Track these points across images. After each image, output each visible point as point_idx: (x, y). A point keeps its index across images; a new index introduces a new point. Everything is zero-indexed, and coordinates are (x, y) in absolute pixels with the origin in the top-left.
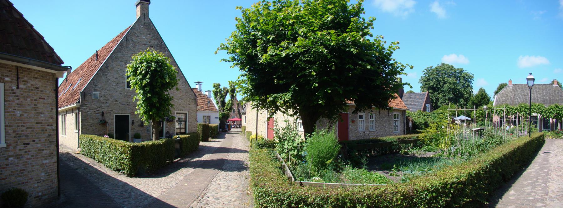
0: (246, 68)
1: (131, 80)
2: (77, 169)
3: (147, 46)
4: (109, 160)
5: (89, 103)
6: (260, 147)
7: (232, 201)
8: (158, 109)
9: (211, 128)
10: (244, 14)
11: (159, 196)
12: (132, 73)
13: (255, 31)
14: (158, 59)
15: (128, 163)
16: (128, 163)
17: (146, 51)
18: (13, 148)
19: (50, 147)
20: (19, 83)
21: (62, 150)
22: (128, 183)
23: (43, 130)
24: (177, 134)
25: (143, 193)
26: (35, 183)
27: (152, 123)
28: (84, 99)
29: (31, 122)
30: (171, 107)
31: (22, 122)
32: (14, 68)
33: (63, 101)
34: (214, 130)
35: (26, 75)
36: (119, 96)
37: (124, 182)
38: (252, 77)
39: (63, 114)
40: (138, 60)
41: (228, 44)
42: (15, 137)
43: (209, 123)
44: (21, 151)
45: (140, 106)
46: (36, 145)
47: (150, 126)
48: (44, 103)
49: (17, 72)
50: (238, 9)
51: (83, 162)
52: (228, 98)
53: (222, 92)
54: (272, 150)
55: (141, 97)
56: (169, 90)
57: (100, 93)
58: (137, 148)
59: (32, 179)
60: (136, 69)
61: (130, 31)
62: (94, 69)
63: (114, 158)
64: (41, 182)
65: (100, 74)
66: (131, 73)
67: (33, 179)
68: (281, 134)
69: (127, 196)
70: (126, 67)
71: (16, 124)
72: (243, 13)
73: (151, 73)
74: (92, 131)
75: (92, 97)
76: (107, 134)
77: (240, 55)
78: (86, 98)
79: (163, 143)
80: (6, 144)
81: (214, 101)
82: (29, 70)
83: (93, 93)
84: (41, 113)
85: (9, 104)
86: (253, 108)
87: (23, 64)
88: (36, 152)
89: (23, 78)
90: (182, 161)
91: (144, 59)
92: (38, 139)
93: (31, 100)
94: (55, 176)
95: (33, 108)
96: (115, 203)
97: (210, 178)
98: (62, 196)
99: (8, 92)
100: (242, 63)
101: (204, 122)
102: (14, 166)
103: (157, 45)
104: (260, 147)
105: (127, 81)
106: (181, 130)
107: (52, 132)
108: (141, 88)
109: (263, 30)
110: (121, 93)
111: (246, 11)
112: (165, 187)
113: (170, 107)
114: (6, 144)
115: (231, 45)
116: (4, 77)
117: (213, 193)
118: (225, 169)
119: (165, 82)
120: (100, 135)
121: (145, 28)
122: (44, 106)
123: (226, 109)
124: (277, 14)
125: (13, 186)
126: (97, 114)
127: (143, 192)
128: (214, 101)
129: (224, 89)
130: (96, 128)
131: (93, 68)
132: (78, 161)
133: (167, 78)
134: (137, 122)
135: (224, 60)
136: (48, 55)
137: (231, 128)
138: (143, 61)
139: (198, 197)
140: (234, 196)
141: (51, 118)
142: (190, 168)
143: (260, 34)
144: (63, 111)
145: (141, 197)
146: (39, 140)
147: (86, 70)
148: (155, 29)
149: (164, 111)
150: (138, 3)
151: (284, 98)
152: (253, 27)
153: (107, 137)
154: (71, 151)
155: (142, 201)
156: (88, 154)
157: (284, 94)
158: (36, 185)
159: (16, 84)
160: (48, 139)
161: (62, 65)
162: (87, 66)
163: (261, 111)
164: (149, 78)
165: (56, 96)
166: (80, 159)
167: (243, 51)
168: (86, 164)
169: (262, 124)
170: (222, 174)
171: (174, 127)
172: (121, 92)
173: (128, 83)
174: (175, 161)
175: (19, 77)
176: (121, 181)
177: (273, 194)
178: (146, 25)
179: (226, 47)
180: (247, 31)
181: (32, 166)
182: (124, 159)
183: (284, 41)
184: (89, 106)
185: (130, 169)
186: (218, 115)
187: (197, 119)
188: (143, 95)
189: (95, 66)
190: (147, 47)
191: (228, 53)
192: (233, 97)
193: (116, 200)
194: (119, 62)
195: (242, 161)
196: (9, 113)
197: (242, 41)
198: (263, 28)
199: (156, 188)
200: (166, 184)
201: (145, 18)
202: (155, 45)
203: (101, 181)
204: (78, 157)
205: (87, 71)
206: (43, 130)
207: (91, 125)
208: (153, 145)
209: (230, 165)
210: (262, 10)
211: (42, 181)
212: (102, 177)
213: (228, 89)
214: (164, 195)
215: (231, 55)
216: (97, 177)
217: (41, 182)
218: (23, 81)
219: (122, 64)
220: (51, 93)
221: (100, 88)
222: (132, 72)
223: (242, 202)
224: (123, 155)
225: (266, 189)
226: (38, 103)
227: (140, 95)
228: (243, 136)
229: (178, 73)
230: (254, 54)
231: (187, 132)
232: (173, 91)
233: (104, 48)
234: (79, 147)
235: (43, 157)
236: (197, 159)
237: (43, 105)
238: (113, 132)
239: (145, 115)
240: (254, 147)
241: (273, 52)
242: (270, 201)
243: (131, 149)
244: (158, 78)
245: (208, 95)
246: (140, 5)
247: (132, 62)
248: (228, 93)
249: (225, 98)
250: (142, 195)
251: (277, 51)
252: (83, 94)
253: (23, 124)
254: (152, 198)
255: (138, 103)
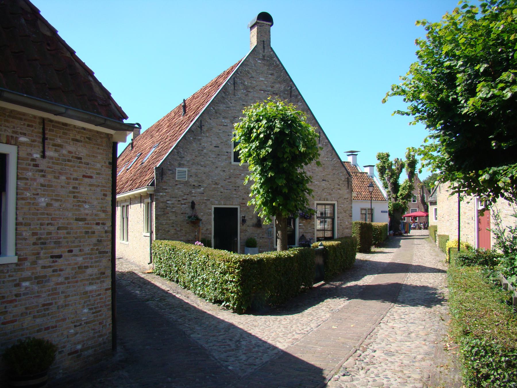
0: (437, 124)
1: (240, 149)
2: (148, 300)
3: (267, 92)
4: (203, 283)
5: (169, 186)
6: (464, 263)
7: (416, 360)
8: (287, 198)
9: (376, 229)
10: (429, 33)
11: (289, 347)
12: (242, 138)
13: (452, 60)
14: (285, 114)
15: (235, 289)
16: (235, 289)
17: (266, 101)
18: (31, 265)
19: (100, 261)
20: (46, 148)
21: (120, 267)
22: (236, 323)
23: (87, 233)
24: (319, 240)
25: (261, 342)
26: (70, 328)
27: (276, 220)
28: (162, 180)
29: (66, 218)
30: (308, 193)
31: (50, 217)
32: (38, 120)
33: (124, 182)
34: (381, 233)
35: (59, 135)
36: (221, 175)
37: (228, 322)
38: (449, 139)
39: (125, 204)
40: (252, 116)
41: (404, 86)
42: (35, 244)
43: (372, 221)
44: (45, 270)
45: (255, 192)
46: (74, 258)
47: (272, 226)
48: (90, 185)
49: (44, 129)
50: (420, 25)
51: (159, 288)
52: (403, 178)
53: (393, 167)
54: (491, 269)
55: (258, 176)
56: (304, 166)
57: (188, 171)
58: (251, 264)
59: (64, 320)
60: (250, 130)
61: (240, 68)
62: (180, 130)
63: (211, 280)
64: (81, 325)
65: (189, 138)
66: (241, 137)
67: (67, 321)
68: (508, 239)
69: (233, 346)
70: (233, 128)
71: (38, 220)
72: (427, 32)
73: (274, 138)
74: (175, 234)
75: (175, 177)
76: (200, 239)
77: (427, 102)
78: (165, 178)
79: (295, 255)
80: (17, 257)
81: (379, 183)
82: (65, 127)
83: (177, 169)
84: (85, 202)
85: (26, 184)
86: (452, 194)
87: (55, 115)
88: (74, 272)
89: (54, 140)
90: (327, 286)
91: (263, 114)
92: (79, 248)
93: (67, 178)
94: (107, 313)
95: (70, 192)
96: (213, 359)
97: (375, 317)
98: (119, 348)
99: (25, 162)
100: (430, 116)
101: (362, 218)
102: (31, 297)
103: (283, 92)
104: (464, 263)
105: (234, 150)
106: (326, 234)
107: (104, 235)
108: (257, 162)
109: (466, 56)
110: (224, 171)
111: (434, 28)
112: (298, 332)
113: (306, 193)
114: (17, 257)
115: (410, 86)
116: (17, 136)
117: (383, 344)
118: (403, 302)
119: (297, 153)
120: (188, 241)
121: (264, 65)
122: (90, 190)
123: (400, 196)
124: (491, 25)
125: (28, 335)
126: (183, 205)
127: (260, 340)
128: (379, 183)
129: (396, 162)
130: (182, 230)
131: (177, 129)
132: (149, 287)
133: (301, 145)
134: (251, 219)
135: (399, 112)
136: (101, 103)
137: (410, 228)
138: (261, 118)
139: (356, 351)
140: (421, 351)
141: (103, 210)
142: (341, 299)
143: (460, 63)
144: (125, 200)
145: (256, 349)
146: (80, 250)
147: (165, 130)
148: (280, 66)
149: (296, 201)
150: (253, 23)
151: (512, 173)
152: (447, 54)
153: (200, 245)
154: (137, 268)
155: (259, 357)
156: (166, 275)
157: (511, 167)
158: (72, 331)
159: (41, 149)
160: (96, 248)
161: (125, 121)
162: (168, 124)
163: (467, 198)
164: (270, 146)
165: (112, 174)
166: (152, 282)
167: (431, 95)
168: (163, 291)
169: (467, 221)
170: (398, 310)
171: (314, 228)
172: (225, 169)
173: (237, 154)
174: (315, 285)
175: (46, 136)
176: (223, 321)
177: (500, 352)
178: (265, 58)
179: (402, 90)
180: (437, 62)
181: (65, 296)
182: (229, 282)
183: (506, 70)
184: (170, 191)
185: (239, 300)
186: (387, 207)
187: (351, 213)
188: (260, 175)
189: (181, 124)
190: (268, 94)
191: (405, 100)
192: (412, 175)
193: (214, 354)
194: (221, 118)
195: (432, 289)
196: (24, 200)
197: (428, 79)
198: (465, 52)
199: (283, 333)
200: (300, 326)
201: (264, 48)
202: (281, 91)
203: (189, 320)
204: (149, 280)
205: (167, 132)
206: (87, 232)
207: (173, 223)
208: (278, 259)
209: (411, 294)
210: (461, 23)
211: (83, 324)
212: (190, 315)
213: (404, 161)
214: (297, 345)
215: (411, 103)
216: (182, 313)
217: (81, 325)
218: (54, 145)
219: (226, 123)
220: (104, 168)
221: (189, 161)
222: (242, 135)
223: (435, 363)
224: (227, 275)
225: (486, 342)
226: (79, 184)
227: (255, 174)
228: (431, 242)
229: (320, 138)
230: (452, 98)
231: (336, 236)
232: (311, 167)
233: (196, 96)
234: (151, 262)
235: (87, 280)
236: (353, 282)
237: (88, 188)
238: (210, 235)
239: (264, 208)
240: (453, 262)
241: (488, 92)
242: (495, 365)
243: (241, 265)
244: (286, 146)
245: (369, 174)
246: (256, 27)
247: (242, 120)
248: (403, 169)
249: (398, 177)
250: (259, 346)
251: (495, 90)
252: (161, 171)
253: (52, 220)
254: (275, 351)
255: (253, 187)
